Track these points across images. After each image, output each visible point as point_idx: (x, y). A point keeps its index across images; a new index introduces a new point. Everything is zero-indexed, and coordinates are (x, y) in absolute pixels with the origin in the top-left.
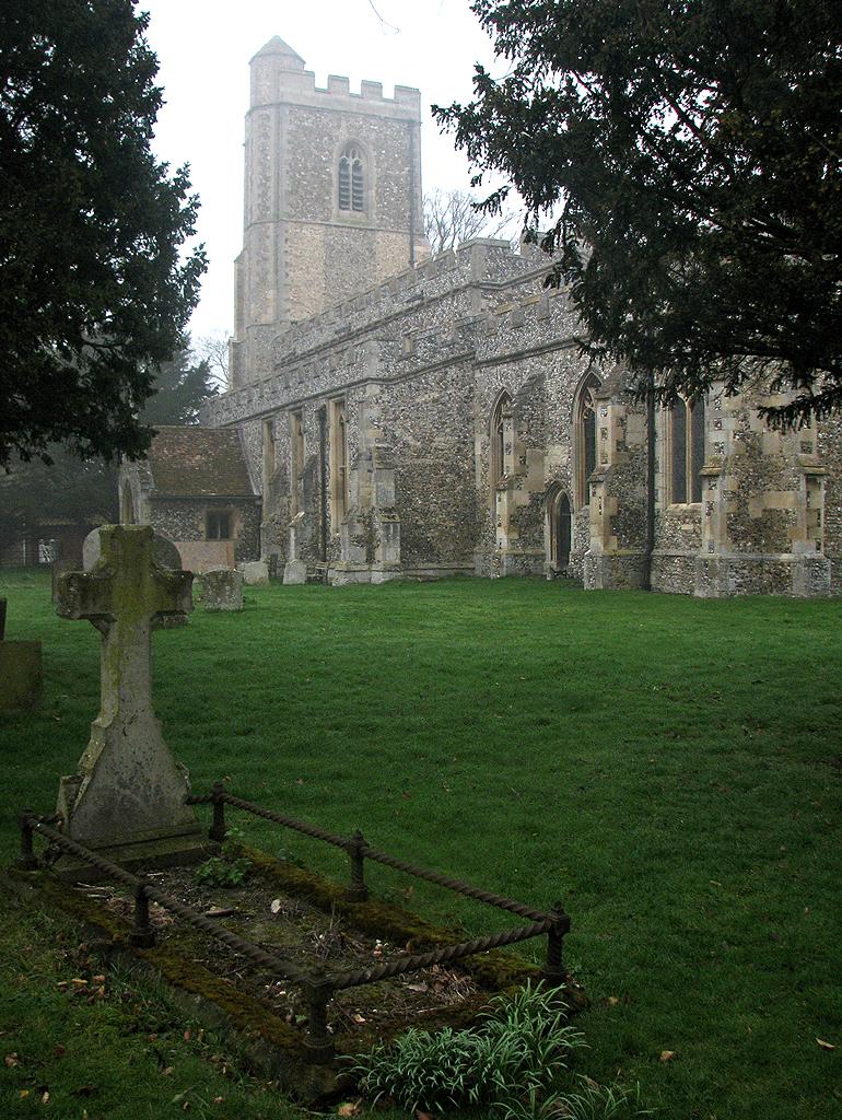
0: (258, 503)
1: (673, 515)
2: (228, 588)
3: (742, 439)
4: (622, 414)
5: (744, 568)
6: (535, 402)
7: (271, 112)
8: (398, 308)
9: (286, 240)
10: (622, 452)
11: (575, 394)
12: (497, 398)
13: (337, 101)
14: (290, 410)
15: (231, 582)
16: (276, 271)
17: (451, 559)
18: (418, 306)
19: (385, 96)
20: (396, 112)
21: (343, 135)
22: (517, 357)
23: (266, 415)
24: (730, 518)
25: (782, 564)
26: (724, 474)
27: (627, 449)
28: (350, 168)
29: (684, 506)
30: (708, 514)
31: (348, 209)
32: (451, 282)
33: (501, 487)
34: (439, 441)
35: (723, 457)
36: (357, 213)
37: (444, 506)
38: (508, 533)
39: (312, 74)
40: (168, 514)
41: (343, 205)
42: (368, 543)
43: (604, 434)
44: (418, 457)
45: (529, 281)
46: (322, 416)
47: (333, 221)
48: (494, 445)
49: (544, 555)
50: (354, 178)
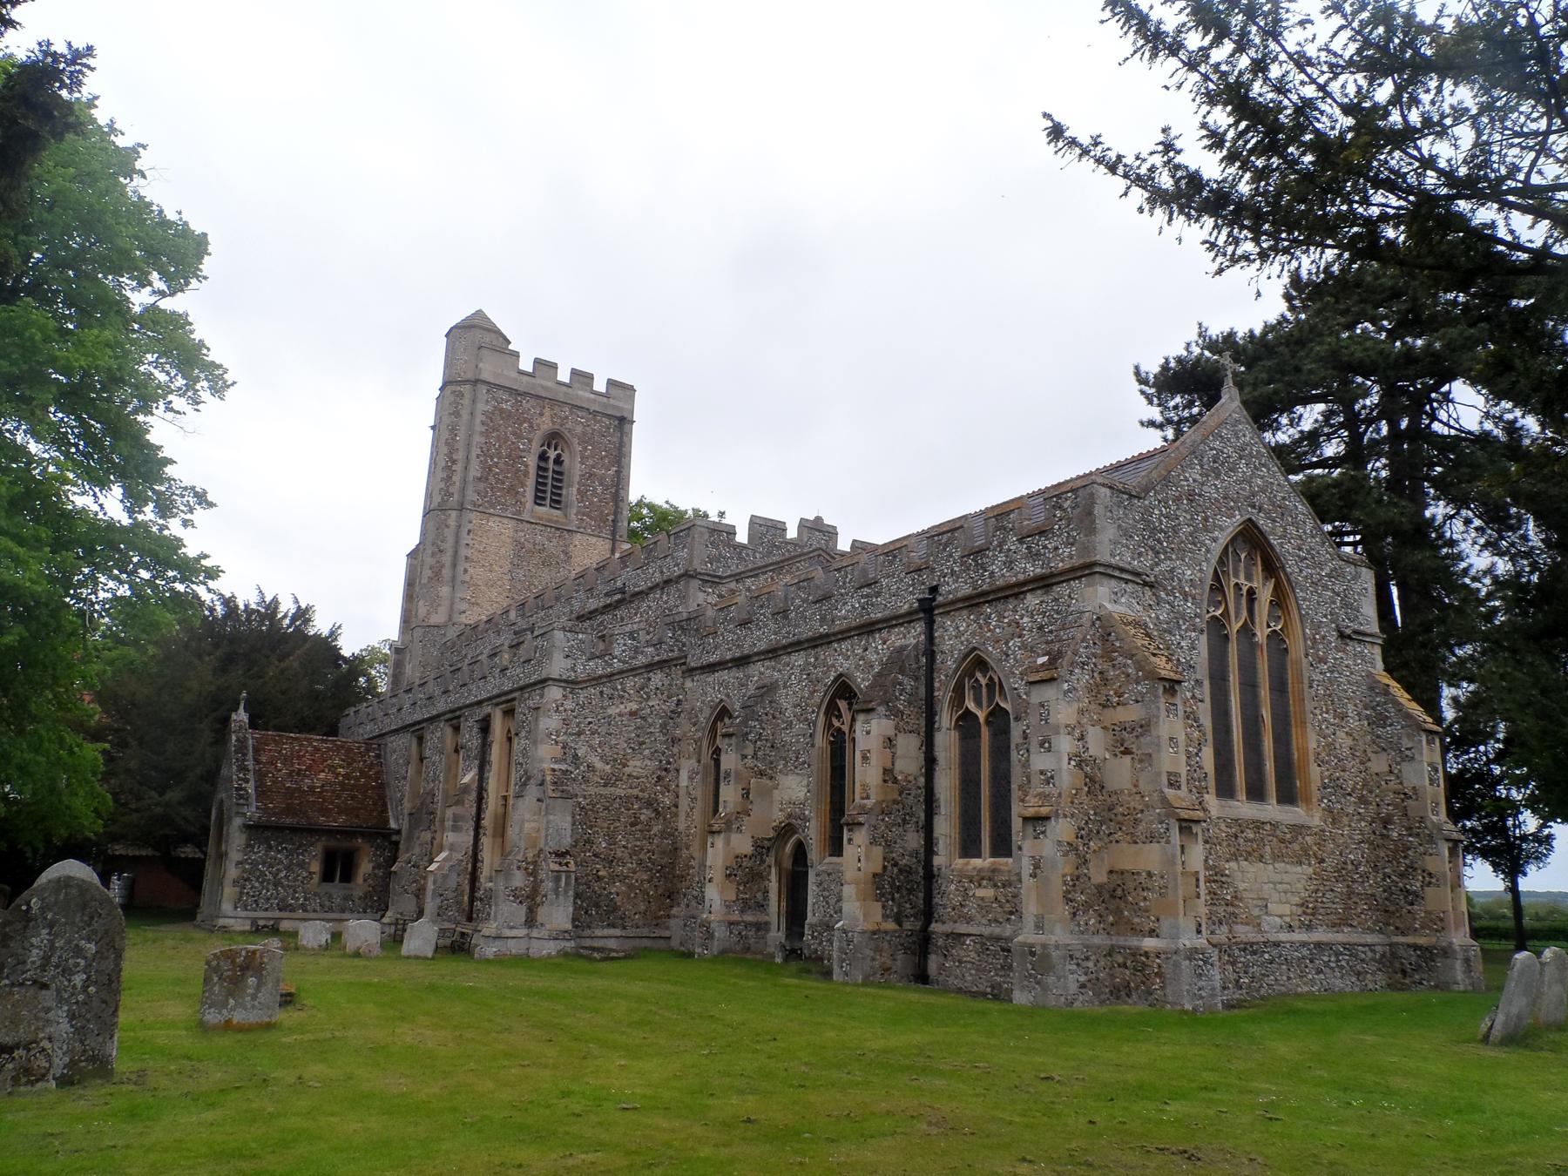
0: (394, 838)
1: (962, 874)
2: (252, 981)
3: (1079, 765)
4: (891, 733)
5: (1087, 959)
6: (764, 717)
7: (466, 389)
8: (593, 604)
9: (469, 531)
10: (890, 784)
11: (819, 708)
12: (711, 714)
13: (542, 387)
14: (447, 721)
15: (259, 971)
16: (454, 566)
17: (641, 923)
18: (619, 602)
19: (596, 388)
20: (606, 406)
21: (546, 424)
22: (742, 661)
23: (417, 727)
24: (1065, 883)
25: (1146, 954)
26: (1057, 816)
27: (895, 781)
28: (551, 461)
29: (977, 862)
30: (1034, 875)
31: (544, 505)
32: (662, 572)
33: (716, 827)
34: (635, 766)
35: (1055, 792)
36: (553, 511)
37: (634, 853)
38: (721, 892)
39: (516, 355)
40: (270, 848)
41: (539, 500)
42: (531, 900)
43: (865, 758)
44: (605, 785)
45: (756, 575)
46: (485, 727)
47: (526, 517)
48: (705, 777)
49: (767, 923)
50: (554, 471)
